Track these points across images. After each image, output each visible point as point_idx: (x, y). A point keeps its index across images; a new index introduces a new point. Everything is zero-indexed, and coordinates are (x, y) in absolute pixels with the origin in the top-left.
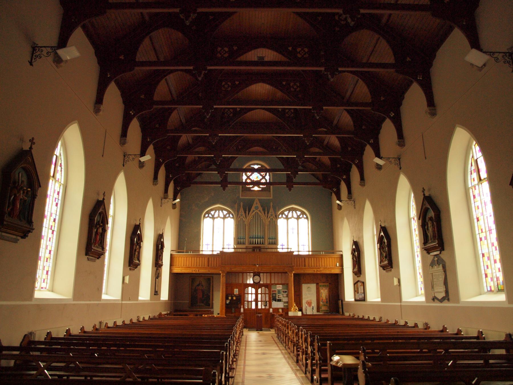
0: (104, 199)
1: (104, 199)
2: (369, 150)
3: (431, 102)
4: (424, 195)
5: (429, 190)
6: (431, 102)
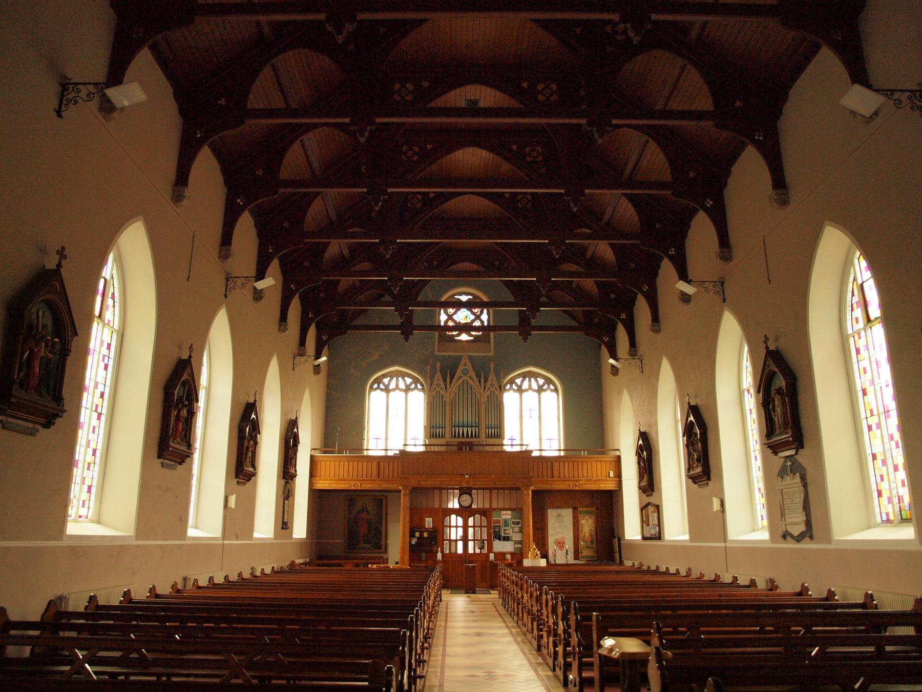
0: (190, 357)
1: (190, 357)
2: (667, 268)
3: (779, 182)
4: (767, 348)
5: (777, 339)
6: (779, 182)
